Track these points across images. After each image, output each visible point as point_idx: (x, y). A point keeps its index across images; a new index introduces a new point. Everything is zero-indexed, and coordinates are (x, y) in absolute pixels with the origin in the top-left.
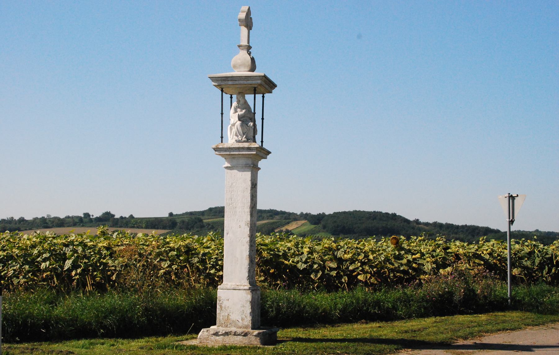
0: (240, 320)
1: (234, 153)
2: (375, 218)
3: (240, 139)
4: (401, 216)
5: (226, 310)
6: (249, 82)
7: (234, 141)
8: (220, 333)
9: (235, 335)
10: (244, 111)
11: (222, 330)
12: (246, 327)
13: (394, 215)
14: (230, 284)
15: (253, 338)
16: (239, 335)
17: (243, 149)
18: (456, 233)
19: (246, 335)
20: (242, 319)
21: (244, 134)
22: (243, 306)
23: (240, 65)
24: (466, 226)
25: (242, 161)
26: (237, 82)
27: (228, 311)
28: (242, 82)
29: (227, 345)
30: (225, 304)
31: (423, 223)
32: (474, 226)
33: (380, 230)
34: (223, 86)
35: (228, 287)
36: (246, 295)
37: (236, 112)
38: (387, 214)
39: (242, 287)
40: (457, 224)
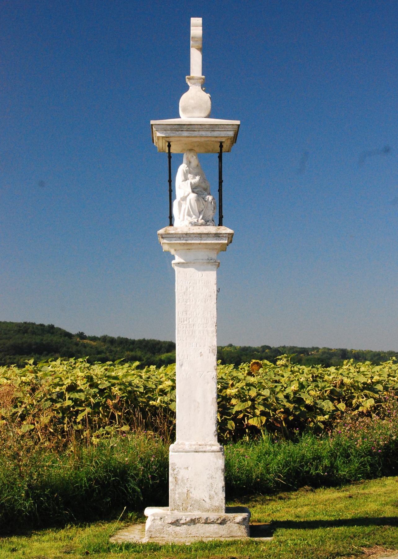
0: (207, 500)
1: (193, 242)
2: (26, 332)
3: (196, 220)
4: (60, 329)
5: (185, 484)
6: (216, 134)
7: (186, 223)
8: (182, 522)
9: (206, 523)
10: (198, 178)
11: (185, 516)
12: (217, 510)
13: (52, 327)
14: (187, 443)
15: (235, 527)
16: (213, 523)
17: (208, 235)
18: (132, 350)
19: (223, 522)
20: (211, 498)
21: (200, 213)
22: (212, 477)
23: (194, 108)
24: (144, 340)
25: (203, 255)
26: (196, 133)
27: (188, 485)
28: (204, 133)
29: (205, 540)
30: (183, 474)
31: (89, 337)
32: (154, 340)
33: (34, 347)
34: (171, 139)
35: (187, 448)
36: (215, 460)
37: (186, 179)
38: (42, 325)
39: (208, 448)
40: (132, 338)
